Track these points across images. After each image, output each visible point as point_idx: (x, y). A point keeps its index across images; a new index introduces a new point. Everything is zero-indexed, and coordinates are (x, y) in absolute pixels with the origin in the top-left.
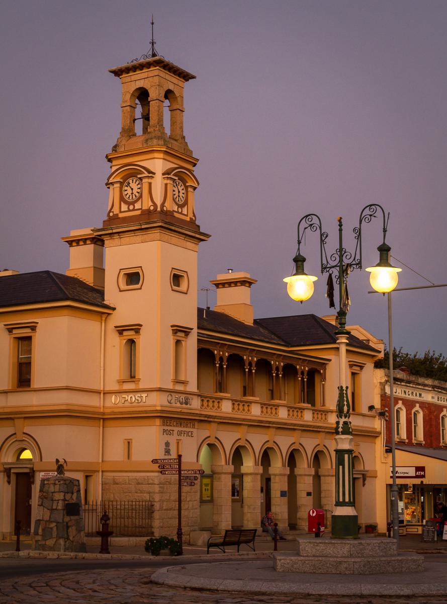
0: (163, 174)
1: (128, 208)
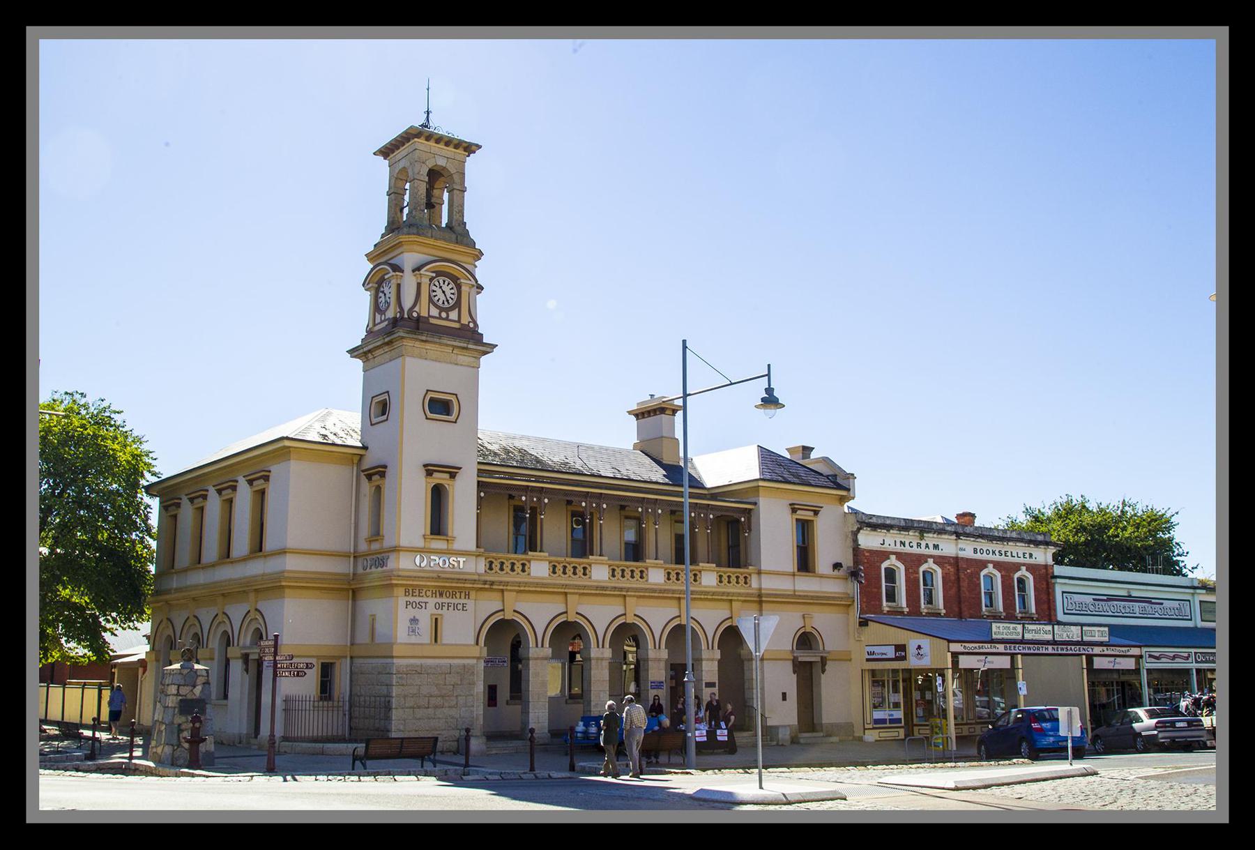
1: (440, 314)
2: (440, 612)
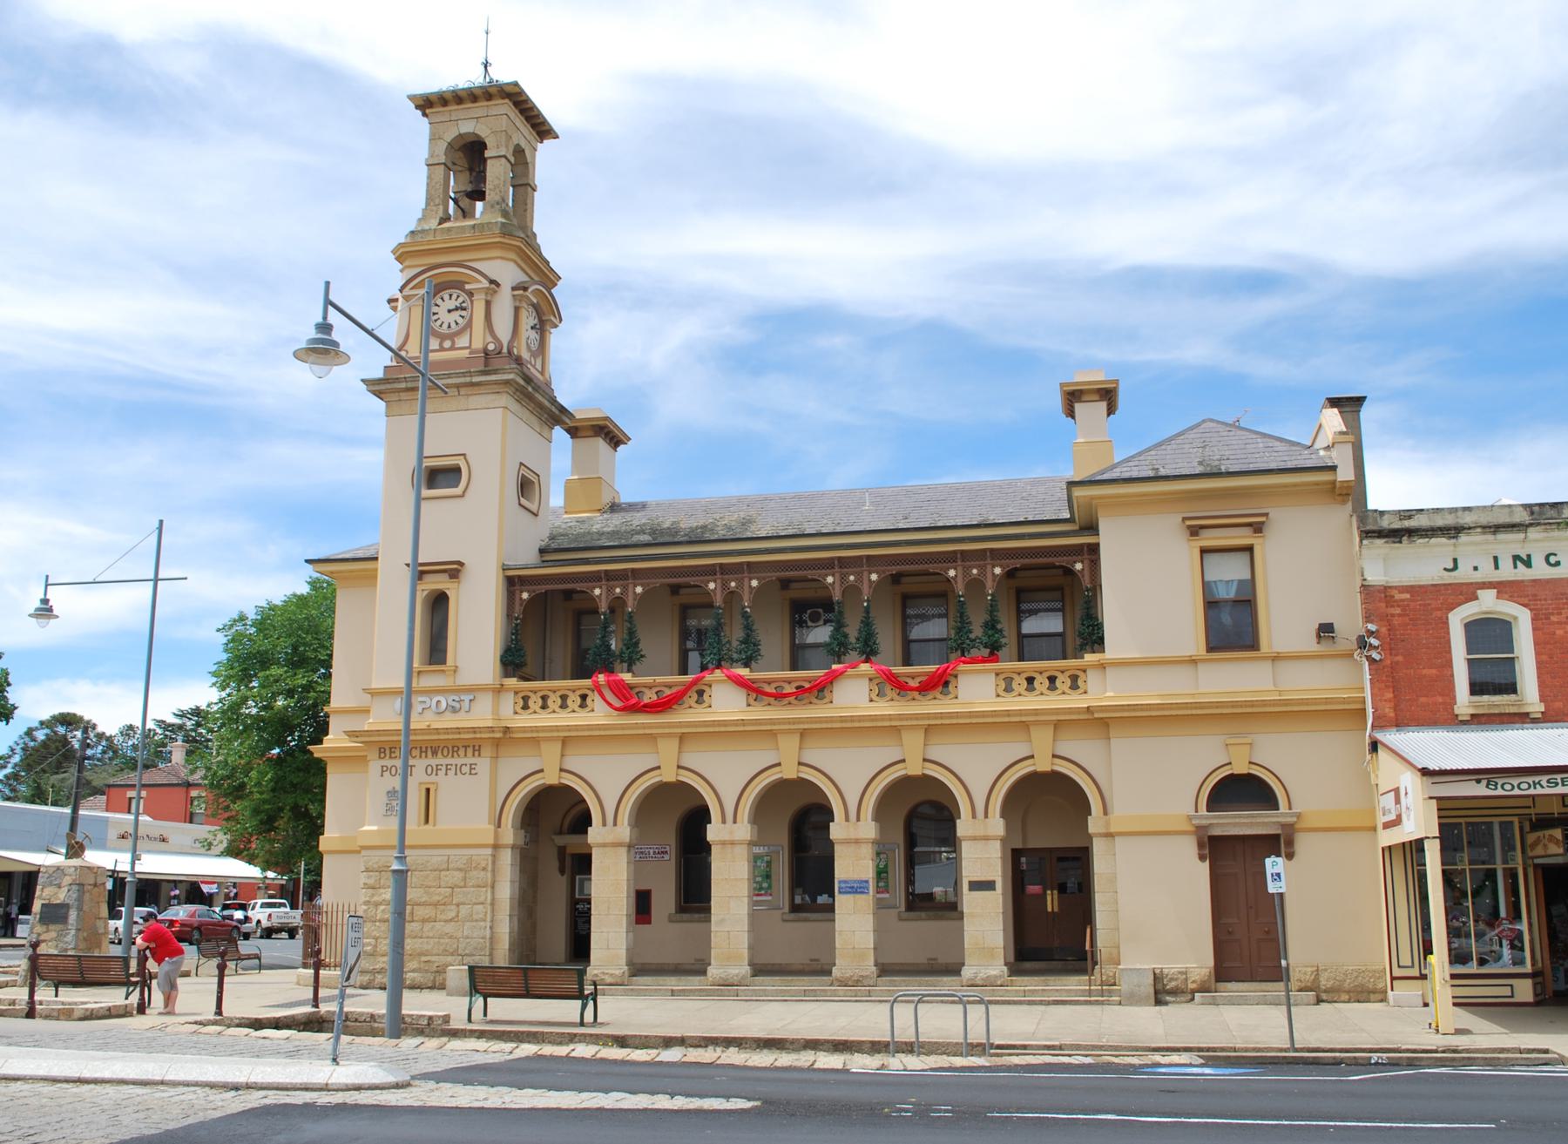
0: (514, 289)
1: (441, 344)
2: (433, 778)
